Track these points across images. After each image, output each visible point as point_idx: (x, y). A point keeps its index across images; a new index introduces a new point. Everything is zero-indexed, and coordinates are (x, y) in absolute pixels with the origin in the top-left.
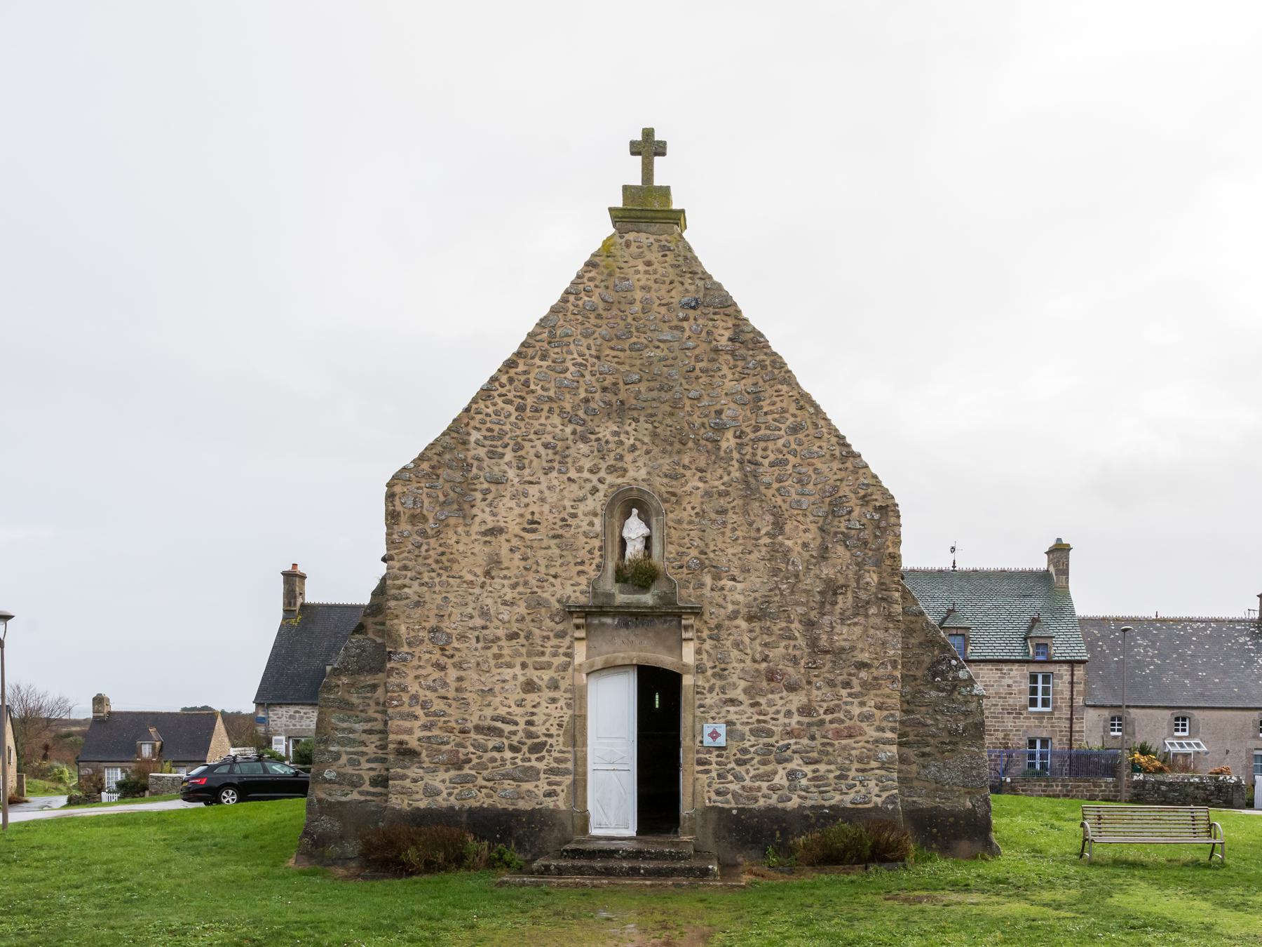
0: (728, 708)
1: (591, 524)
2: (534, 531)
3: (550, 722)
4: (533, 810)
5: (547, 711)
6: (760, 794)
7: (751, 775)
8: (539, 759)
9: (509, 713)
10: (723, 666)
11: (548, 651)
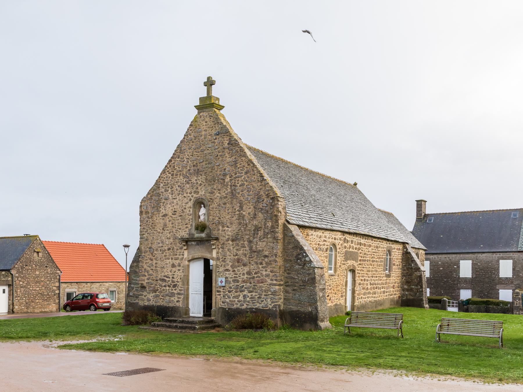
0: (226, 272)
1: (190, 211)
2: (175, 214)
3: (178, 277)
4: (173, 306)
5: (178, 274)
6: (235, 303)
7: (232, 296)
8: (175, 290)
9: (168, 274)
10: (225, 257)
11: (178, 254)
